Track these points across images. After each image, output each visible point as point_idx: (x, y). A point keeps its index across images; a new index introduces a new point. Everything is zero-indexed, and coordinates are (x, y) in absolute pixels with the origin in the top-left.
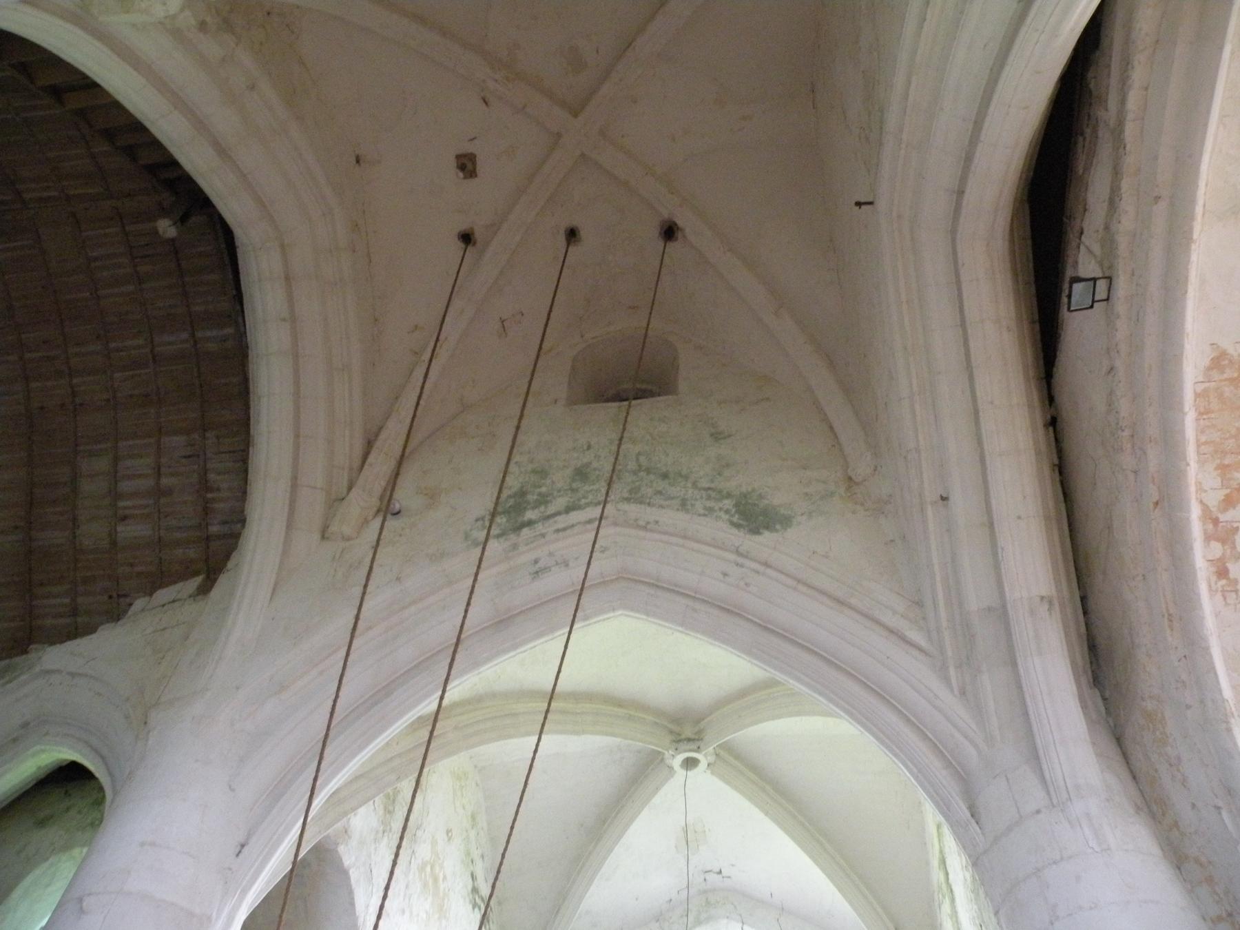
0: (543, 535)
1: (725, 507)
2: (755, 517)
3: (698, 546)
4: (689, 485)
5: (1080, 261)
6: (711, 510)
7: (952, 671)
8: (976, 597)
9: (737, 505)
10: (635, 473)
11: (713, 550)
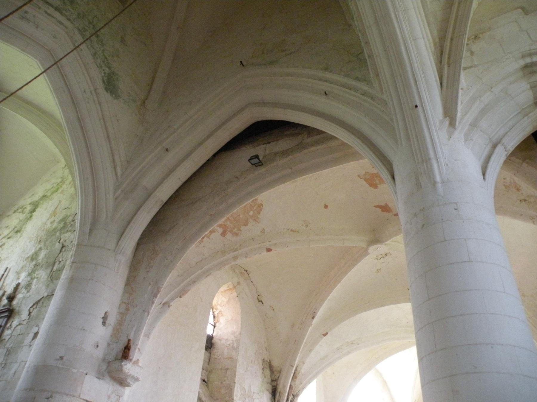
0: (40, 8)
1: (106, 71)
2: (110, 85)
3: (84, 73)
4: (102, 49)
5: (261, 146)
6: (101, 67)
7: (120, 191)
8: (148, 181)
9: (109, 74)
10: (90, 23)
11: (88, 79)
